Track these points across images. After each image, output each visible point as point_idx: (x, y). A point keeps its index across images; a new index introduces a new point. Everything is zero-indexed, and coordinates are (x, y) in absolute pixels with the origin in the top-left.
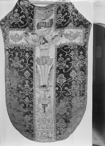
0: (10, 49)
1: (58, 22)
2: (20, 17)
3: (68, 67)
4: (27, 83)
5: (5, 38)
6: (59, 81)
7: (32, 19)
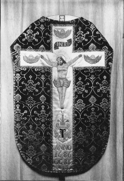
0: (21, 71)
1: (79, 40)
2: (34, 34)
3: (87, 92)
4: (43, 108)
5: (14, 59)
6: (78, 107)
7: (49, 35)
